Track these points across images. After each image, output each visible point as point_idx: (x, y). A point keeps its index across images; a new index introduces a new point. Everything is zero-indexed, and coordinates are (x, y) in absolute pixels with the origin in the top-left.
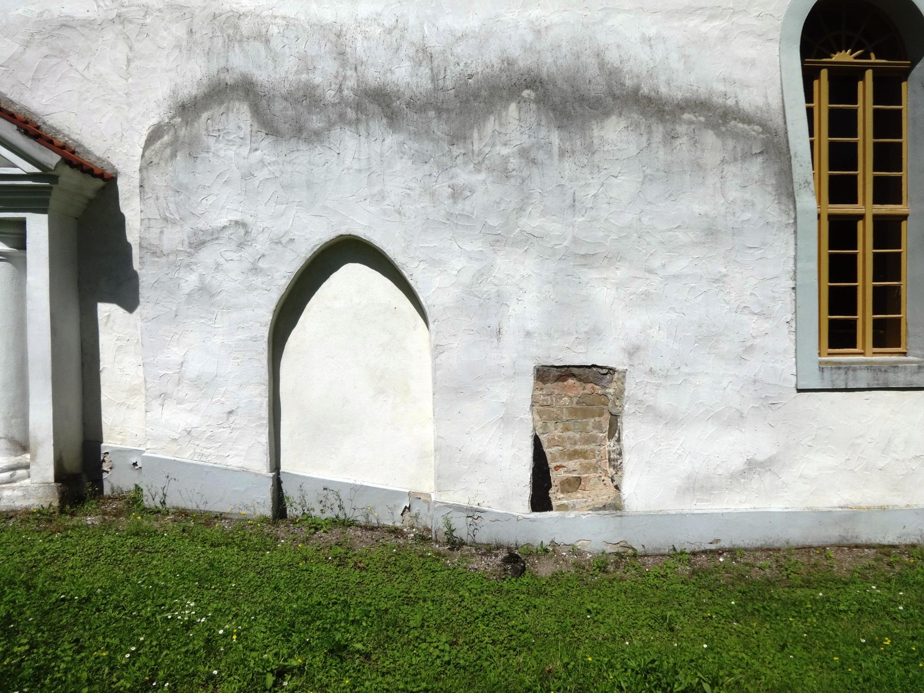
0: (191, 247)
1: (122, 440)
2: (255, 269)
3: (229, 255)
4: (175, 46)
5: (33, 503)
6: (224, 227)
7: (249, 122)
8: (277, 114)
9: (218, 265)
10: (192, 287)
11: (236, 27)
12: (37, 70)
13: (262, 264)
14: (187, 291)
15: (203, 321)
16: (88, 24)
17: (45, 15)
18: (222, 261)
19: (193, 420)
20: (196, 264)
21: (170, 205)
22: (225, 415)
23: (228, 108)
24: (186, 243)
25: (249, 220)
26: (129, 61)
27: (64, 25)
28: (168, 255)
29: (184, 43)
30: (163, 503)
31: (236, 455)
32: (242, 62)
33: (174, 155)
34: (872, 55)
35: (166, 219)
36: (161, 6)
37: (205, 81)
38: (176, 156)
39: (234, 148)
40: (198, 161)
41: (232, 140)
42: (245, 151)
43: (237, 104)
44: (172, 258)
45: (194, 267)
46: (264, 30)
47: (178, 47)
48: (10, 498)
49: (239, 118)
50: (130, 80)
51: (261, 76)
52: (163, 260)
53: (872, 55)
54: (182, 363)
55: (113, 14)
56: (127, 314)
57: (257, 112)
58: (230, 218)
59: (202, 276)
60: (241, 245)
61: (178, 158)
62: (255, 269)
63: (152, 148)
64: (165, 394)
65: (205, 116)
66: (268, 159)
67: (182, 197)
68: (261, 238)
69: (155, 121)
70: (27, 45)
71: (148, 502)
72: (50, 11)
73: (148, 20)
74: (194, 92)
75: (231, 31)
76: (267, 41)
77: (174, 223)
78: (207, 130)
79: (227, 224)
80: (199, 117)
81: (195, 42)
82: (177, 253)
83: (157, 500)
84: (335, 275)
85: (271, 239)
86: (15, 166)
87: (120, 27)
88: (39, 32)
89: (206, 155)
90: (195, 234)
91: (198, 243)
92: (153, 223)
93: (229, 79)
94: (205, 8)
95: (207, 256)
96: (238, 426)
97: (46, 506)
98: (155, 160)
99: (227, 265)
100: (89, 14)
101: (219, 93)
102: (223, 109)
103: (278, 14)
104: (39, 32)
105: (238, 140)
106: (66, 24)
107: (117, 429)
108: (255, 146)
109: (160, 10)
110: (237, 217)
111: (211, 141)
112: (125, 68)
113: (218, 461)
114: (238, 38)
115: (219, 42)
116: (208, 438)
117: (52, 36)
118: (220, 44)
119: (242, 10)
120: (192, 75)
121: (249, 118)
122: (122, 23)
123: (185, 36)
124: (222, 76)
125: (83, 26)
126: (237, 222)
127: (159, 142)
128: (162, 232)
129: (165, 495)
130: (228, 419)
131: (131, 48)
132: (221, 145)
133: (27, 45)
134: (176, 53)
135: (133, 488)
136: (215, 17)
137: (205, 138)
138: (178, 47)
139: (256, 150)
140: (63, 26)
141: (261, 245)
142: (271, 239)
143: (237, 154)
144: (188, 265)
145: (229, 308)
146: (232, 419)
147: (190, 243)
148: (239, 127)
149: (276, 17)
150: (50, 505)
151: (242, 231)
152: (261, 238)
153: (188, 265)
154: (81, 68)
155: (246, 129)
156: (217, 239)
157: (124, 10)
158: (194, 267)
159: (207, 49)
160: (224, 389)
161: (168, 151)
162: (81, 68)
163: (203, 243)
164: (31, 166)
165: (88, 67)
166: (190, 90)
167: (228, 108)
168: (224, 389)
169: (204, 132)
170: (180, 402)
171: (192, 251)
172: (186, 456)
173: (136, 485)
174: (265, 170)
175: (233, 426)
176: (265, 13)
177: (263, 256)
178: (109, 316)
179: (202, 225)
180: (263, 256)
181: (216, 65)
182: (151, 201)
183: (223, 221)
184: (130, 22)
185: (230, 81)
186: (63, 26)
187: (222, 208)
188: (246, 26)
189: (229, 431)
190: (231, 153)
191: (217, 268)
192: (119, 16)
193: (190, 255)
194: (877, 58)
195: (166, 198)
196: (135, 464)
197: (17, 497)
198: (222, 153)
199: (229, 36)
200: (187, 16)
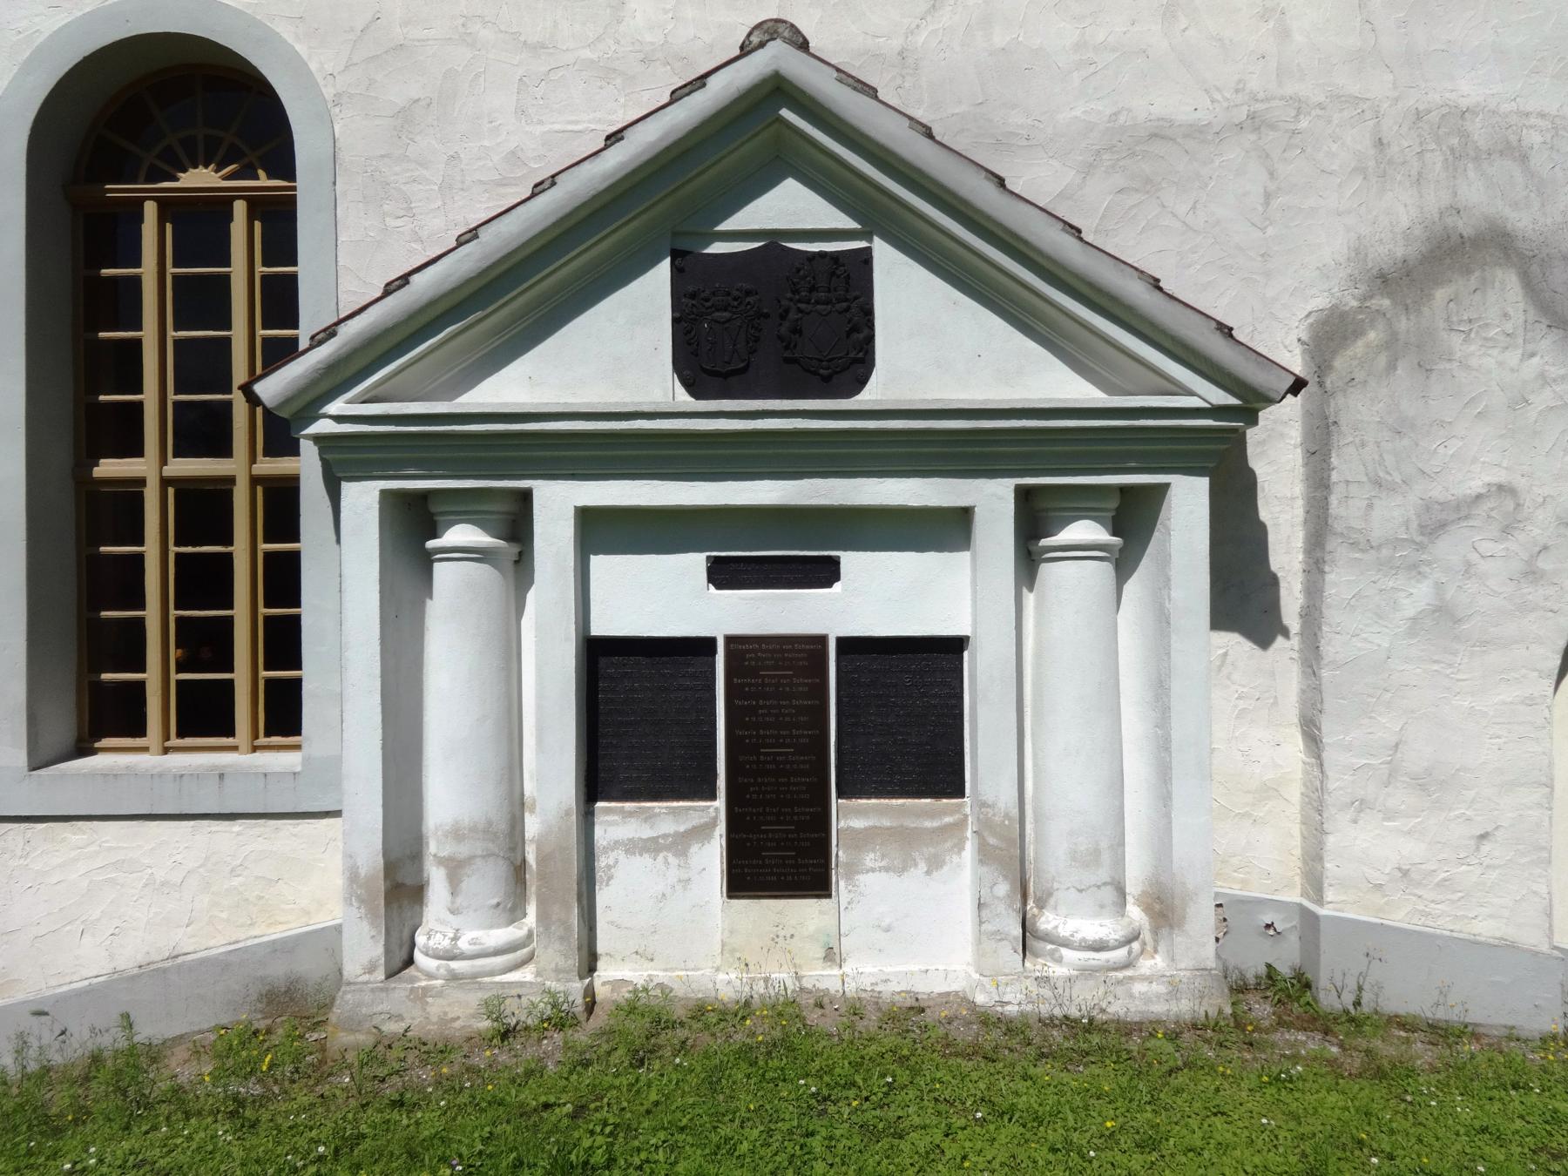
0: (1422, 534)
1: (1243, 881)
2: (1532, 574)
3: (1487, 547)
4: (1355, 170)
5: (1185, 1007)
6: (1479, 497)
7: (1521, 306)
8: (1560, 290)
9: (1469, 565)
10: (1422, 605)
11: (1465, 135)
12: (1103, 216)
13: (1544, 564)
14: (1411, 612)
15: (1436, 667)
16: (1196, 132)
17: (1122, 119)
18: (1474, 557)
19: (1411, 850)
20: (1429, 563)
21: (1386, 456)
22: (1472, 842)
23: (1484, 281)
24: (1414, 525)
25: (1521, 483)
26: (1268, 197)
27: (1156, 135)
28: (1379, 547)
29: (1372, 163)
30: (1357, 1003)
31: (1491, 916)
32: (1480, 196)
33: (1392, 367)
34: (261, 173)
35: (1378, 483)
36: (1322, 99)
37: (1418, 231)
38: (1395, 368)
39: (1495, 352)
40: (1434, 376)
41: (1491, 339)
42: (1513, 357)
43: (1499, 273)
44: (1385, 552)
45: (1424, 569)
46: (1513, 138)
47: (1360, 170)
48: (1147, 999)
49: (1505, 296)
50: (1270, 231)
51: (1523, 221)
52: (1370, 556)
53: (261, 173)
54: (1397, 745)
55: (1242, 114)
56: (1257, 651)
57: (1530, 287)
58: (1488, 479)
59: (1439, 586)
60: (1507, 530)
61: (1399, 372)
62: (1532, 574)
63: (1349, 353)
64: (1362, 801)
65: (1441, 295)
66: (1553, 371)
67: (1406, 442)
68: (1540, 515)
69: (1321, 302)
70: (1087, 170)
71: (1328, 1000)
72: (1130, 110)
73: (1304, 124)
74: (1400, 252)
75: (1455, 141)
76: (1524, 159)
77: (1392, 489)
78: (1448, 319)
79: (1483, 491)
80: (1430, 297)
81: (1390, 162)
82: (1396, 543)
83: (1348, 999)
84: (932, 554)
85: (1558, 518)
86: (1191, 393)
87: (1253, 137)
88: (1110, 149)
89: (1448, 366)
90: (1428, 509)
91: (1436, 522)
92: (1353, 489)
93: (1465, 226)
94: (1397, 100)
95: (1449, 548)
96: (1497, 862)
97: (1213, 1013)
98: (1360, 376)
99: (1484, 566)
100: (1198, 115)
101: (1452, 254)
102: (1473, 281)
103: (1529, 109)
104: (1110, 149)
105: (1502, 338)
106: (1160, 133)
107: (1234, 860)
108: (1530, 347)
109: (1321, 106)
110: (1500, 477)
111: (1456, 339)
112: (1260, 209)
113: (1456, 927)
114: (1472, 153)
115: (1436, 160)
116: (1441, 884)
117: (1134, 154)
118: (1439, 166)
119: (1464, 103)
120: (1396, 218)
121: (1520, 298)
122: (1257, 129)
123: (1372, 152)
124: (1449, 221)
125: (1185, 136)
126: (1500, 487)
127: (1360, 343)
128: (1370, 506)
129: (1360, 988)
130: (1478, 849)
131: (1272, 174)
132: (1473, 348)
133: (1087, 170)
134: (1358, 181)
135: (1263, 970)
136: (1419, 116)
137: (1444, 335)
138: (1360, 170)
139: (1533, 355)
140: (1154, 136)
141: (1540, 527)
142: (1558, 518)
143: (1500, 364)
144: (1414, 566)
145: (1484, 643)
146: (1486, 847)
147: (1421, 526)
148: (1506, 315)
149: (1527, 115)
150: (1220, 1012)
151: (1509, 504)
152: (1540, 515)
153: (1414, 566)
154: (1182, 209)
155: (1518, 317)
156: (1467, 517)
157: (1259, 106)
158: (1424, 569)
159: (1414, 173)
160: (1472, 793)
161: (1382, 360)
162: (1182, 209)
163: (1443, 525)
164: (1221, 392)
165: (1194, 208)
166: (1390, 248)
167: (1484, 281)
168: (1472, 793)
169: (1442, 324)
170: (1390, 815)
171: (1425, 540)
172: (1400, 916)
173: (1269, 966)
174: (1547, 392)
175: (1487, 861)
176: (1506, 107)
177: (1545, 548)
178: (1225, 654)
179: (1437, 492)
180: (1545, 548)
181: (1435, 200)
182: (1351, 449)
183: (1476, 485)
184: (1273, 127)
185: (1468, 232)
186: (1154, 136)
187: (1475, 460)
188: (1478, 130)
189: (1479, 871)
190: (1489, 362)
191: (1466, 571)
192: (1252, 116)
193: (1421, 547)
194: (270, 177)
195: (1378, 444)
196: (1268, 926)
197: (1158, 996)
198: (1474, 362)
199: (1452, 150)
200: (1368, 115)
